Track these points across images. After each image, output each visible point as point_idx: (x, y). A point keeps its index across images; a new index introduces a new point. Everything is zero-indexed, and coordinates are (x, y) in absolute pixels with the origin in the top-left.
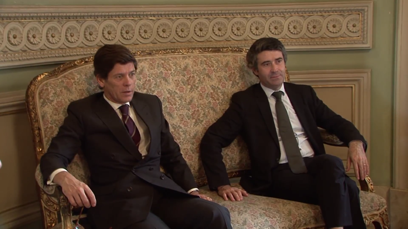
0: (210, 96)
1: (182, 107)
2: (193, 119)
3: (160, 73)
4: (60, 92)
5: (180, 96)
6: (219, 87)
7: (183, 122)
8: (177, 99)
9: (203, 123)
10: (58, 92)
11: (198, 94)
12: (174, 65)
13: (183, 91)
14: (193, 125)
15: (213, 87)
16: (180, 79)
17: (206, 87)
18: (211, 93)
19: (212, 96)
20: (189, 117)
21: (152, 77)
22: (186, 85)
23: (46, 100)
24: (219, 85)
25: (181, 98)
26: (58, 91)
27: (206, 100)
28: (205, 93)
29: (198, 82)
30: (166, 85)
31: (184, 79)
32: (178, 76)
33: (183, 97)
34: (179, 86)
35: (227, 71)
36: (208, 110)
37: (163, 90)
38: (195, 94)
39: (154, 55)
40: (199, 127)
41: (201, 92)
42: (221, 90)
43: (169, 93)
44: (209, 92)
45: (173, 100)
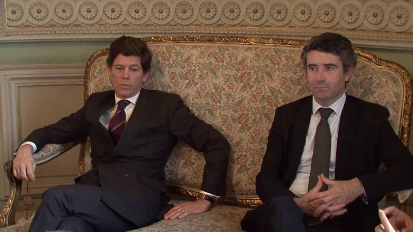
0: (266, 100)
1: (227, 107)
2: (239, 123)
3: (208, 63)
4: (385, 82)
5: (227, 94)
6: (280, 91)
7: (226, 124)
8: (223, 97)
9: (251, 131)
10: (383, 82)
11: (251, 95)
12: (229, 57)
13: (233, 89)
14: (238, 130)
15: (272, 89)
16: (232, 74)
17: (263, 87)
18: (269, 96)
19: (268, 100)
20: (234, 120)
21: (198, 66)
22: (238, 81)
23: (368, 91)
24: (170, 82)
25: (228, 96)
26: (383, 81)
27: (260, 103)
28: (384, 101)
29: (254, 80)
30: (213, 79)
31: (356, 80)
32: (230, 70)
33: (231, 95)
34: (175, 79)
35: (239, 70)
36: (261, 116)
37: (208, 83)
38: (247, 95)
39: (214, 42)
40: (245, 134)
41: (98, 84)
42: (282, 95)
43: (271, 91)
44: (265, 95)
45: (218, 97)
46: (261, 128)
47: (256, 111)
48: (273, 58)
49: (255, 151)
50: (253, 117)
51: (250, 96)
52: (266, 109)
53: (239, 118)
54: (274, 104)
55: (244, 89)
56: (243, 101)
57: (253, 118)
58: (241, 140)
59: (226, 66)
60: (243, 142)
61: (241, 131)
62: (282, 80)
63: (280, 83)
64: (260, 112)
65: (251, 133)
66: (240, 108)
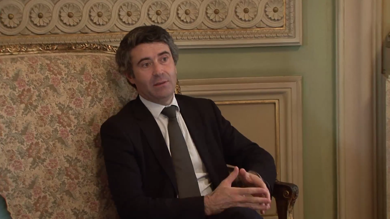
0: (56, 121)
2: (30, 156)
5: (7, 121)
9: (45, 163)
18: (58, 115)
19: (59, 120)
20: (22, 155)
22: (17, 103)
29: (36, 98)
38: (40, 171)
40: (39, 169)
43: (60, 108)
46: (57, 158)
47: (38, 84)
48: (60, 119)
49: (55, 188)
50: (45, 145)
51: (36, 119)
52: (59, 131)
53: (28, 150)
54: (67, 124)
55: (27, 112)
56: (29, 127)
57: (45, 147)
58: (19, 71)
59: (5, 140)
60: (39, 180)
61: (25, 113)
62: (69, 92)
63: (68, 96)
64: (52, 137)
65: (38, 113)
66: (27, 138)
